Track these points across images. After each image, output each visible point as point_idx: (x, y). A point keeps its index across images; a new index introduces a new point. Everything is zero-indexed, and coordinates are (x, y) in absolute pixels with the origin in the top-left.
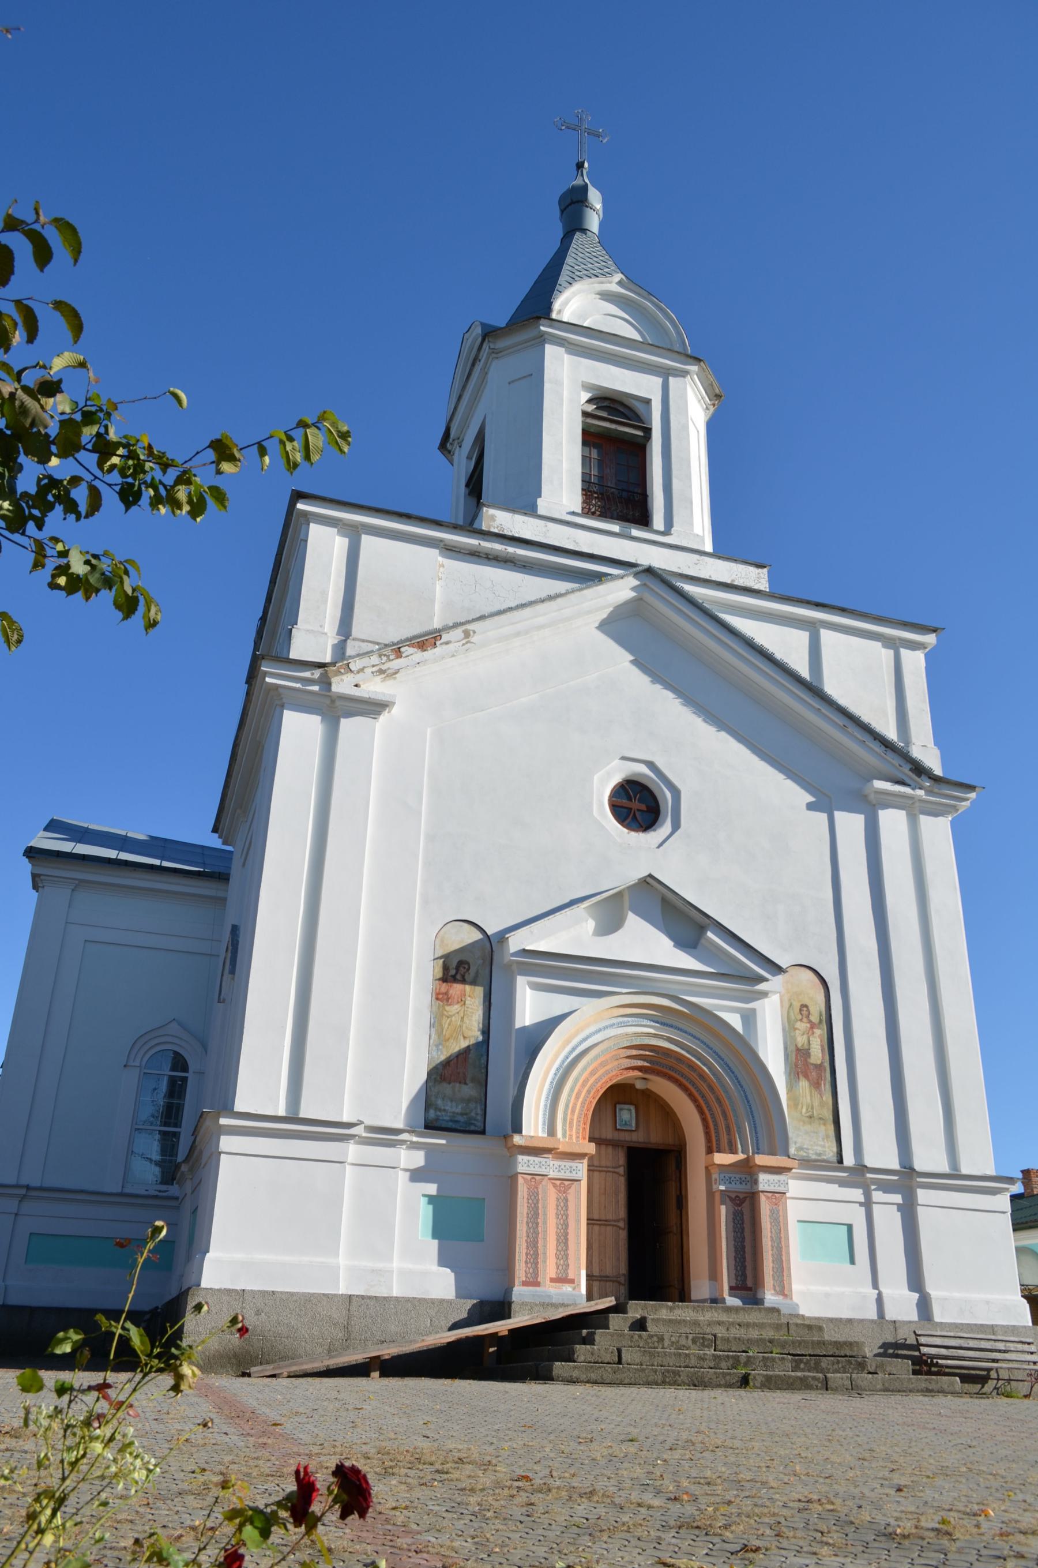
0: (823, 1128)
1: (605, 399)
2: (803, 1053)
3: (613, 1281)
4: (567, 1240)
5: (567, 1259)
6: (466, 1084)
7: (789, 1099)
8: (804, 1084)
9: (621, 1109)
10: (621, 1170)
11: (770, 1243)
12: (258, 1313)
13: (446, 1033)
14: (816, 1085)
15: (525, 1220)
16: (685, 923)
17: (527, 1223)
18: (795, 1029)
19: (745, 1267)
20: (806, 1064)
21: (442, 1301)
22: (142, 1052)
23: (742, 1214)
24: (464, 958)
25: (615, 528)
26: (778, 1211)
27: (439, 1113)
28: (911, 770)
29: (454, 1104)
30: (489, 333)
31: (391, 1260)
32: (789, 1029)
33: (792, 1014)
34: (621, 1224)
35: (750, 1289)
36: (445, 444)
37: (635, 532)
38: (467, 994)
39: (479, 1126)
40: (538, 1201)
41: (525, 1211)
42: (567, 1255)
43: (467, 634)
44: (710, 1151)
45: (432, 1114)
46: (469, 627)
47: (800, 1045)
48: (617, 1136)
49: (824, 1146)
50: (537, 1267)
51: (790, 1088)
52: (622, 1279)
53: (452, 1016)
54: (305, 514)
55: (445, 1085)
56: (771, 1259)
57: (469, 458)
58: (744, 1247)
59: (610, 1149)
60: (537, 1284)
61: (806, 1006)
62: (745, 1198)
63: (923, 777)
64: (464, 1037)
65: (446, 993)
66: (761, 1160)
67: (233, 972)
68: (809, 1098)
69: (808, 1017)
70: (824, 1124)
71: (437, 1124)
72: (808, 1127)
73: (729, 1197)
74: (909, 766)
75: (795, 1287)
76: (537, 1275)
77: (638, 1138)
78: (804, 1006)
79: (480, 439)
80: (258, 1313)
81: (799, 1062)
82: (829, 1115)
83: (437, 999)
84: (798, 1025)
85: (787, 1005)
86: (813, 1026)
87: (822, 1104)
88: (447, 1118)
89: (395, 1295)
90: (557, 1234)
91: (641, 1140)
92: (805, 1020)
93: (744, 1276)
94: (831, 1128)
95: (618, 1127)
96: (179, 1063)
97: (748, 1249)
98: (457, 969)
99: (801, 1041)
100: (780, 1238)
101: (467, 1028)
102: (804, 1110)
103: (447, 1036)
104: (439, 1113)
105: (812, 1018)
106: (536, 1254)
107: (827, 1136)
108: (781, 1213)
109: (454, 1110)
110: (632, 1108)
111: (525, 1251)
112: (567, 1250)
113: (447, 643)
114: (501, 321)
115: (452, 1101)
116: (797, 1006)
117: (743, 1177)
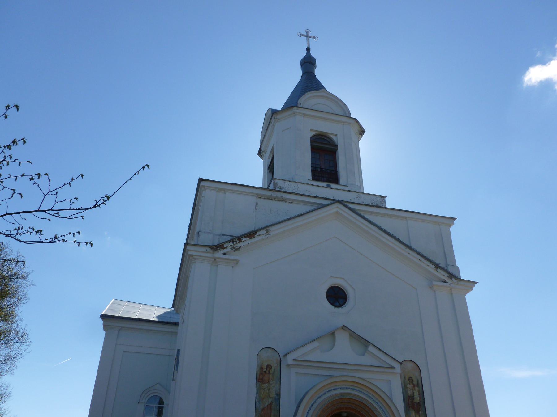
1: (319, 135)
2: (411, 398)
8: (412, 412)
22: (147, 395)
25: (325, 184)
30: (274, 113)
32: (404, 388)
36: (260, 153)
37: (333, 186)
43: (267, 231)
46: (268, 228)
47: (410, 394)
54: (204, 187)
57: (269, 158)
61: (411, 378)
65: (262, 379)
67: (177, 370)
69: (412, 382)
74: (447, 275)
78: (410, 378)
79: (272, 151)
83: (259, 381)
96: (161, 402)
98: (266, 368)
99: (410, 392)
113: (259, 235)
114: (279, 108)
116: (407, 378)
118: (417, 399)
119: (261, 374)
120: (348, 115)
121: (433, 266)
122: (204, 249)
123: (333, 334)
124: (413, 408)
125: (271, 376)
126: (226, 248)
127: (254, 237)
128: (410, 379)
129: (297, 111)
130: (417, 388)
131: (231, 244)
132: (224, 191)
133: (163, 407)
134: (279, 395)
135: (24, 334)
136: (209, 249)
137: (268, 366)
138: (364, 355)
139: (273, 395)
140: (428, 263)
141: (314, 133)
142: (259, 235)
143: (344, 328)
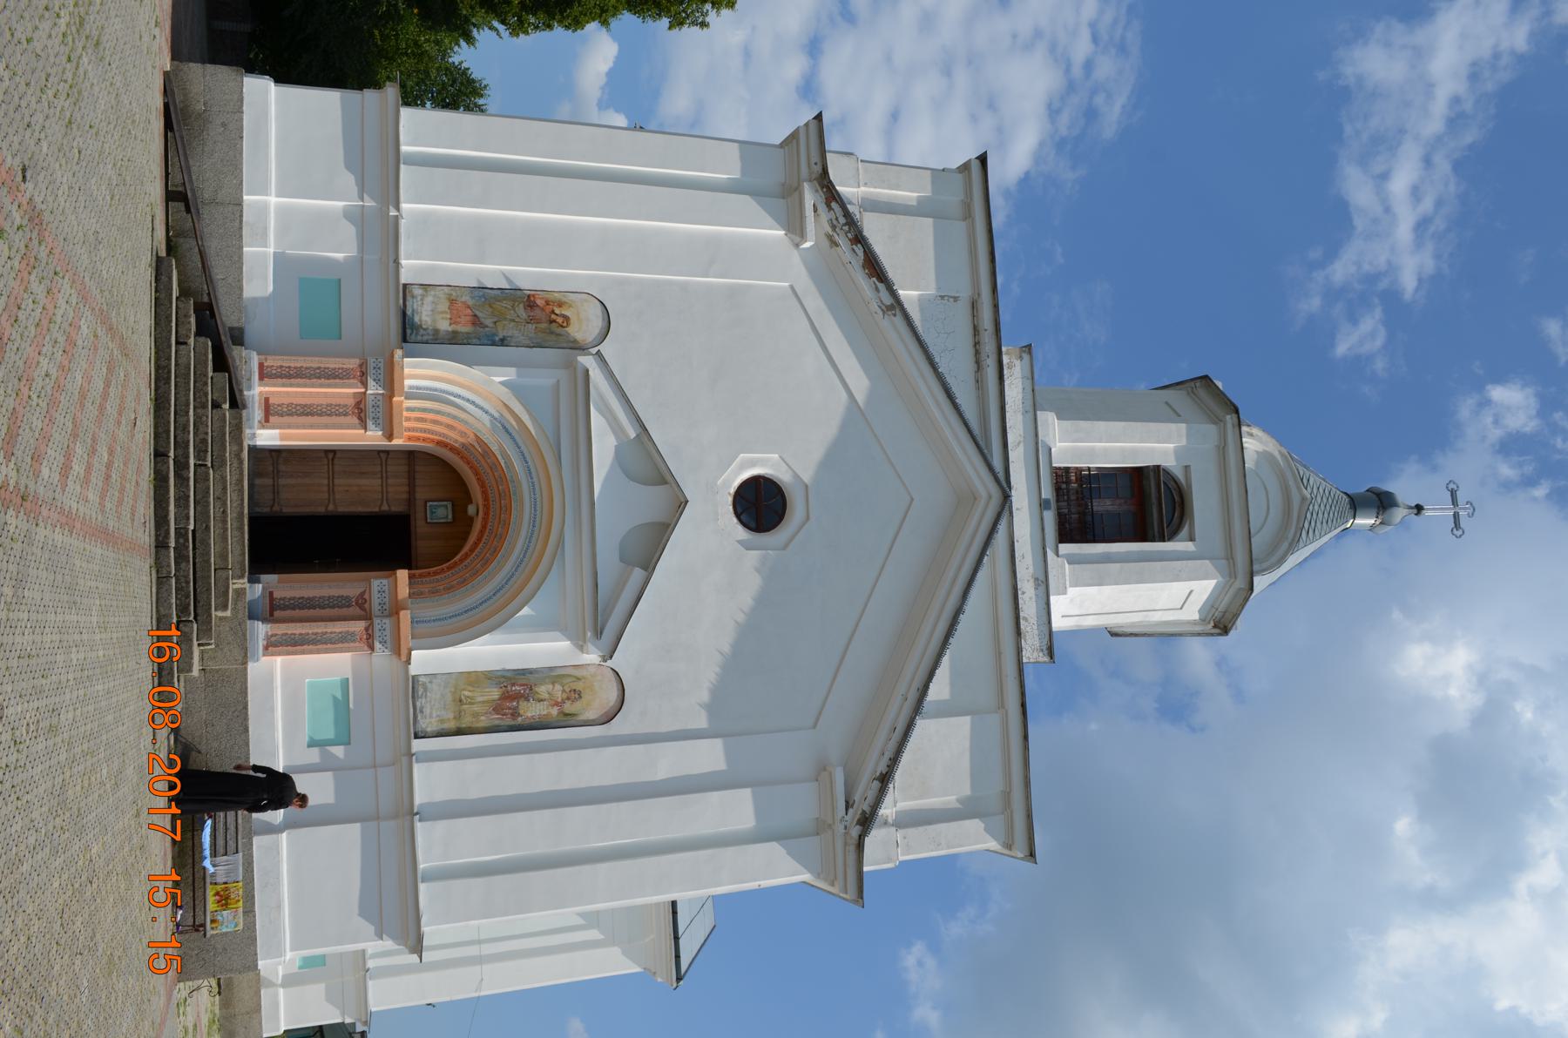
0: (451, 716)
8: (495, 693)
10: (385, 508)
12: (224, 125)
13: (498, 305)
14: (497, 709)
16: (648, 547)
20: (517, 697)
21: (241, 289)
28: (864, 812)
31: (278, 196)
32: (552, 675)
34: (331, 507)
35: (271, 614)
43: (890, 308)
45: (418, 291)
52: (276, 508)
59: (405, 496)
60: (261, 378)
63: (858, 828)
66: (405, 616)
72: (449, 698)
74: (866, 808)
75: (279, 661)
76: (271, 376)
77: (420, 527)
80: (224, 125)
82: (466, 722)
87: (476, 715)
89: (260, 963)
93: (285, 608)
94: (452, 725)
97: (311, 612)
99: (543, 690)
105: (568, 704)
106: (290, 377)
107: (442, 721)
113: (877, 289)
116: (579, 686)
119: (547, 303)
120: (1256, 567)
121: (882, 768)
122: (815, 157)
123: (664, 482)
124: (507, 697)
125: (543, 325)
126: (830, 208)
127: (870, 276)
128: (576, 695)
129: (1229, 426)
131: (842, 220)
132: (968, 215)
134: (503, 342)
135: (241, 331)
136: (818, 169)
137: (567, 318)
138: (622, 560)
140: (889, 754)
142: (877, 289)
143: (682, 504)
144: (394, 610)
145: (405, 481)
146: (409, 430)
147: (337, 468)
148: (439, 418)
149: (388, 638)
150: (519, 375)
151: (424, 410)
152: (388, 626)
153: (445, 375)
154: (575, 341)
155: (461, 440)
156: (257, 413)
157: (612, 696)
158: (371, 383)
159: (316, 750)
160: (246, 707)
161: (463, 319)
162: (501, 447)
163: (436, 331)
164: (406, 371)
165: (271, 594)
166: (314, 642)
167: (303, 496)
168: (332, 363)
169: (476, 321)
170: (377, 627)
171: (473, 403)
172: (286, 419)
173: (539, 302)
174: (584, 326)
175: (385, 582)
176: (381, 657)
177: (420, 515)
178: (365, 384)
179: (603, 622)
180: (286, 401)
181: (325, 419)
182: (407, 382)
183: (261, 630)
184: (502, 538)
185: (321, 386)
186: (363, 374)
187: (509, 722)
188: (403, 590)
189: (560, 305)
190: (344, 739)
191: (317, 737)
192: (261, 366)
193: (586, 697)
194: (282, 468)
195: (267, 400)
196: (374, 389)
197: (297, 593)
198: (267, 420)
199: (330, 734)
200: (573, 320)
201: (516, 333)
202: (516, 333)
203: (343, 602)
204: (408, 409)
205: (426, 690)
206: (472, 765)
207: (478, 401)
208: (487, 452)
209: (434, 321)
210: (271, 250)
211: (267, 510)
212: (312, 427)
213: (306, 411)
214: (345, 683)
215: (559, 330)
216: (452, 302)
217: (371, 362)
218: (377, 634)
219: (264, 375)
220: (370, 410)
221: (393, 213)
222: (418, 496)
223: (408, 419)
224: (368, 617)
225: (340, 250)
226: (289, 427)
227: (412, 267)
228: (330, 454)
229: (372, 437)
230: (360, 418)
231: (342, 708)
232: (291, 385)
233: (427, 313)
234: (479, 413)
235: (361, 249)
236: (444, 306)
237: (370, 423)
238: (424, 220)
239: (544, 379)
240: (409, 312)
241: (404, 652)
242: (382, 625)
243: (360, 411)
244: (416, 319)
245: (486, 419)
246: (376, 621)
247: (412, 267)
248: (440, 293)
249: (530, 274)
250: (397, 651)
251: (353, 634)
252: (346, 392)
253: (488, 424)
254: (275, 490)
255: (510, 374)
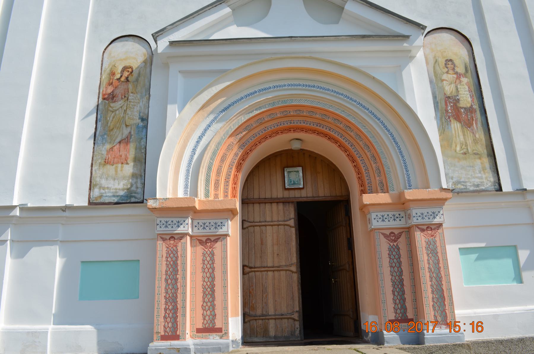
0: (478, 162)
3: (288, 318)
4: (213, 291)
5: (214, 310)
6: (127, 164)
7: (441, 140)
8: (455, 126)
9: (289, 172)
10: (292, 223)
11: (428, 275)
13: (111, 125)
14: (468, 124)
15: (164, 277)
17: (166, 280)
18: (443, 81)
19: (404, 300)
23: (399, 249)
24: (128, 65)
26: (435, 243)
27: (102, 191)
29: (116, 181)
32: (435, 82)
33: (437, 68)
34: (294, 268)
38: (130, 91)
39: (139, 196)
40: (177, 258)
41: (164, 268)
42: (213, 307)
44: (363, 192)
45: (96, 192)
48: (286, 194)
49: (481, 178)
50: (176, 322)
51: (443, 129)
52: (296, 316)
53: (116, 110)
55: (108, 166)
56: (430, 290)
58: (402, 281)
59: (281, 206)
60: (177, 337)
61: (451, 60)
62: (400, 234)
64: (127, 126)
66: (409, 194)
68: (462, 137)
70: (480, 158)
71: (102, 200)
73: (383, 234)
76: (175, 327)
81: (449, 109)
82: (482, 149)
84: (445, 77)
85: (432, 62)
86: (459, 76)
87: (475, 141)
88: (110, 194)
90: (204, 287)
91: (310, 195)
92: (451, 72)
94: (486, 162)
95: (287, 187)
97: (407, 283)
99: (449, 89)
100: (439, 268)
101: (129, 118)
102: (458, 148)
103: (112, 127)
104: (102, 191)
106: (175, 309)
107: (484, 169)
108: (438, 244)
109: (117, 186)
110: (300, 169)
111: (163, 306)
112: (213, 301)
115: (114, 179)
116: (442, 61)
117: (397, 214)
118: (466, 99)
119: (111, 84)
124: (458, 118)
130: (465, 80)
133: (14, 315)
134: (145, 119)
137: (125, 69)
138: (337, 22)
139: (134, 118)
141: (465, 130)
144: (402, 205)
145: (268, 206)
146: (226, 196)
147: (258, 264)
148: (215, 169)
149: (430, 211)
150: (174, 102)
151: (207, 181)
152: (419, 211)
153: (173, 160)
154: (145, 62)
155: (235, 149)
156: (214, 339)
157: (446, 36)
158: (181, 230)
159: (525, 275)
160: (501, 342)
161: (123, 153)
162: (241, 113)
163: (134, 176)
164: (169, 195)
165: (392, 321)
166: (439, 280)
167: (285, 294)
168: (162, 267)
169: (126, 141)
170: (420, 221)
171: (200, 138)
172: (218, 311)
173: (110, 90)
174: (133, 55)
175: (373, 215)
176: (447, 216)
177: (297, 194)
178: (183, 236)
179: (399, 31)
180: (200, 311)
181: (218, 274)
182: (181, 194)
183: (436, 335)
184: (326, 113)
185: (185, 278)
186: (172, 237)
187: (478, 114)
188: (383, 198)
189: (113, 74)
190: (512, 251)
191: (513, 275)
192: (164, 338)
193: (451, 56)
194: (259, 312)
195: (199, 331)
196: (187, 227)
197: (389, 297)
198: (219, 330)
199: (508, 263)
200: (127, 63)
201: (137, 109)
202: (137, 109)
203: (395, 255)
204: (207, 195)
205: (459, 182)
206: (520, 144)
207: (198, 133)
208: (245, 126)
209: (124, 178)
210: (51, 327)
211: (297, 324)
212: (225, 287)
213: (209, 292)
214: (464, 251)
215: (135, 74)
216: (107, 162)
217: (161, 230)
218: (426, 221)
219: (173, 335)
220: (207, 232)
221: (17, 212)
222: (280, 195)
223: (216, 196)
224: (408, 231)
225: (52, 262)
226: (226, 308)
227: (74, 195)
228: (247, 269)
229: (232, 228)
230: (216, 241)
231: (483, 254)
232: (184, 307)
233: (117, 181)
234: (209, 134)
235: (51, 242)
236: (110, 169)
237: (221, 231)
238: (29, 186)
239: (178, 82)
240: (116, 200)
241: (444, 195)
242: (418, 215)
243: (209, 241)
244: (122, 193)
245: (216, 126)
246: (415, 221)
247: (74, 195)
248: (97, 172)
249: (84, 97)
250: (441, 201)
251: (428, 243)
252: (190, 255)
253: (220, 125)
254: (280, 317)
255: (172, 109)
